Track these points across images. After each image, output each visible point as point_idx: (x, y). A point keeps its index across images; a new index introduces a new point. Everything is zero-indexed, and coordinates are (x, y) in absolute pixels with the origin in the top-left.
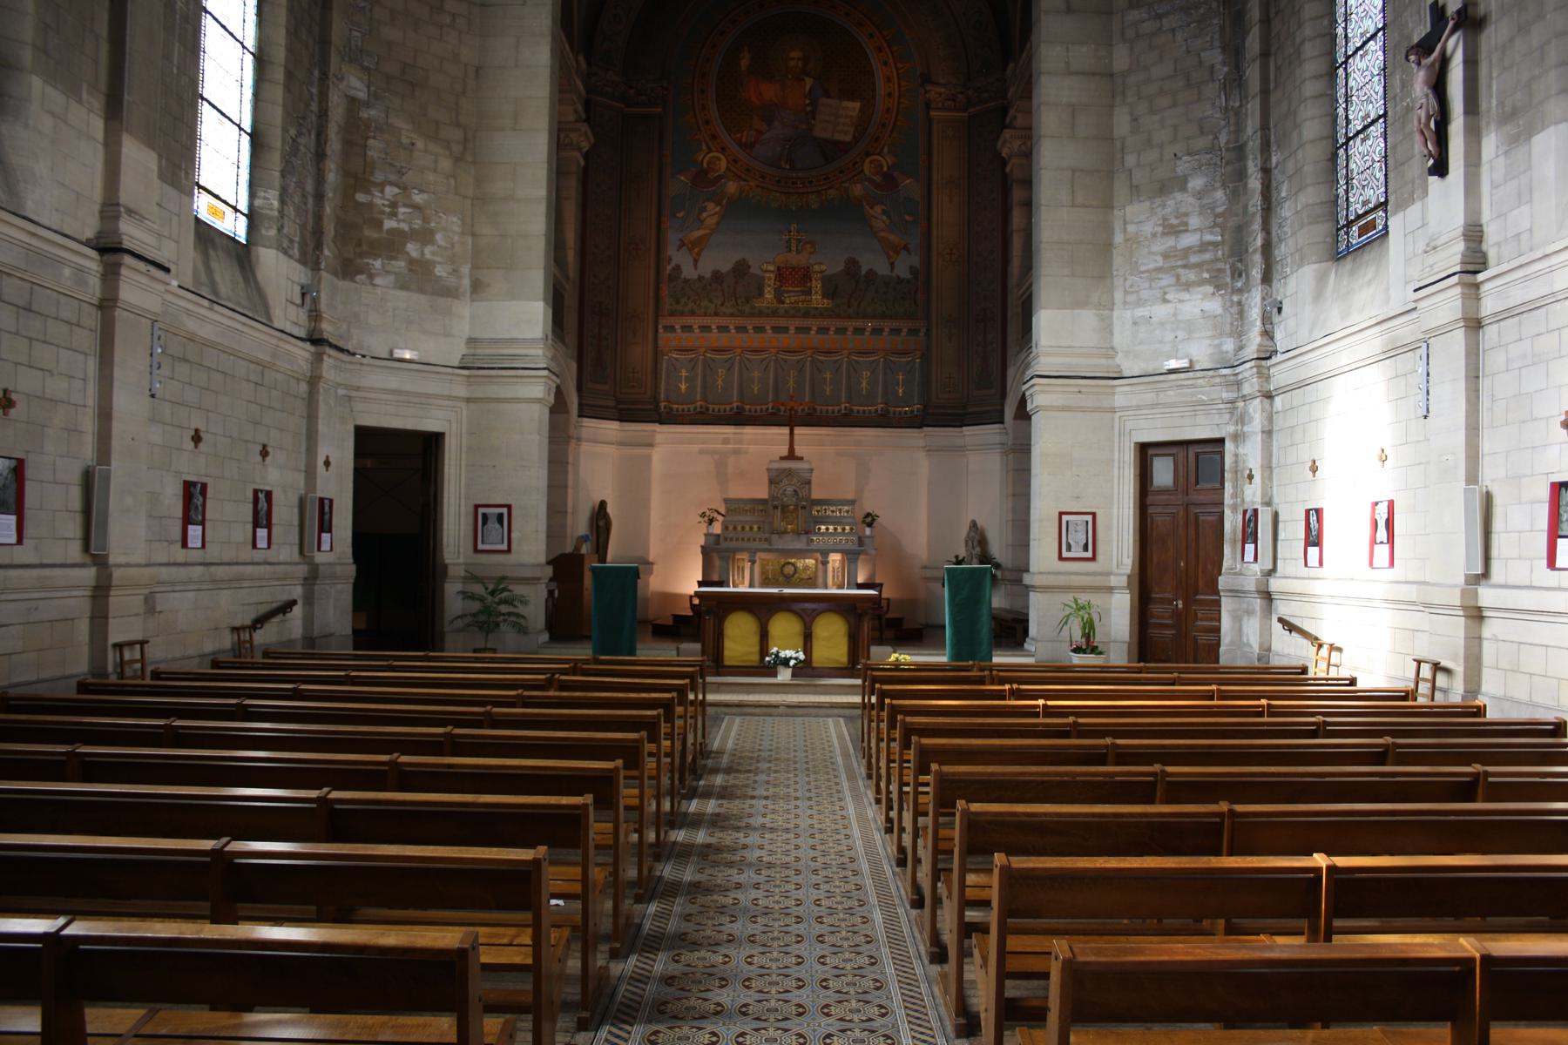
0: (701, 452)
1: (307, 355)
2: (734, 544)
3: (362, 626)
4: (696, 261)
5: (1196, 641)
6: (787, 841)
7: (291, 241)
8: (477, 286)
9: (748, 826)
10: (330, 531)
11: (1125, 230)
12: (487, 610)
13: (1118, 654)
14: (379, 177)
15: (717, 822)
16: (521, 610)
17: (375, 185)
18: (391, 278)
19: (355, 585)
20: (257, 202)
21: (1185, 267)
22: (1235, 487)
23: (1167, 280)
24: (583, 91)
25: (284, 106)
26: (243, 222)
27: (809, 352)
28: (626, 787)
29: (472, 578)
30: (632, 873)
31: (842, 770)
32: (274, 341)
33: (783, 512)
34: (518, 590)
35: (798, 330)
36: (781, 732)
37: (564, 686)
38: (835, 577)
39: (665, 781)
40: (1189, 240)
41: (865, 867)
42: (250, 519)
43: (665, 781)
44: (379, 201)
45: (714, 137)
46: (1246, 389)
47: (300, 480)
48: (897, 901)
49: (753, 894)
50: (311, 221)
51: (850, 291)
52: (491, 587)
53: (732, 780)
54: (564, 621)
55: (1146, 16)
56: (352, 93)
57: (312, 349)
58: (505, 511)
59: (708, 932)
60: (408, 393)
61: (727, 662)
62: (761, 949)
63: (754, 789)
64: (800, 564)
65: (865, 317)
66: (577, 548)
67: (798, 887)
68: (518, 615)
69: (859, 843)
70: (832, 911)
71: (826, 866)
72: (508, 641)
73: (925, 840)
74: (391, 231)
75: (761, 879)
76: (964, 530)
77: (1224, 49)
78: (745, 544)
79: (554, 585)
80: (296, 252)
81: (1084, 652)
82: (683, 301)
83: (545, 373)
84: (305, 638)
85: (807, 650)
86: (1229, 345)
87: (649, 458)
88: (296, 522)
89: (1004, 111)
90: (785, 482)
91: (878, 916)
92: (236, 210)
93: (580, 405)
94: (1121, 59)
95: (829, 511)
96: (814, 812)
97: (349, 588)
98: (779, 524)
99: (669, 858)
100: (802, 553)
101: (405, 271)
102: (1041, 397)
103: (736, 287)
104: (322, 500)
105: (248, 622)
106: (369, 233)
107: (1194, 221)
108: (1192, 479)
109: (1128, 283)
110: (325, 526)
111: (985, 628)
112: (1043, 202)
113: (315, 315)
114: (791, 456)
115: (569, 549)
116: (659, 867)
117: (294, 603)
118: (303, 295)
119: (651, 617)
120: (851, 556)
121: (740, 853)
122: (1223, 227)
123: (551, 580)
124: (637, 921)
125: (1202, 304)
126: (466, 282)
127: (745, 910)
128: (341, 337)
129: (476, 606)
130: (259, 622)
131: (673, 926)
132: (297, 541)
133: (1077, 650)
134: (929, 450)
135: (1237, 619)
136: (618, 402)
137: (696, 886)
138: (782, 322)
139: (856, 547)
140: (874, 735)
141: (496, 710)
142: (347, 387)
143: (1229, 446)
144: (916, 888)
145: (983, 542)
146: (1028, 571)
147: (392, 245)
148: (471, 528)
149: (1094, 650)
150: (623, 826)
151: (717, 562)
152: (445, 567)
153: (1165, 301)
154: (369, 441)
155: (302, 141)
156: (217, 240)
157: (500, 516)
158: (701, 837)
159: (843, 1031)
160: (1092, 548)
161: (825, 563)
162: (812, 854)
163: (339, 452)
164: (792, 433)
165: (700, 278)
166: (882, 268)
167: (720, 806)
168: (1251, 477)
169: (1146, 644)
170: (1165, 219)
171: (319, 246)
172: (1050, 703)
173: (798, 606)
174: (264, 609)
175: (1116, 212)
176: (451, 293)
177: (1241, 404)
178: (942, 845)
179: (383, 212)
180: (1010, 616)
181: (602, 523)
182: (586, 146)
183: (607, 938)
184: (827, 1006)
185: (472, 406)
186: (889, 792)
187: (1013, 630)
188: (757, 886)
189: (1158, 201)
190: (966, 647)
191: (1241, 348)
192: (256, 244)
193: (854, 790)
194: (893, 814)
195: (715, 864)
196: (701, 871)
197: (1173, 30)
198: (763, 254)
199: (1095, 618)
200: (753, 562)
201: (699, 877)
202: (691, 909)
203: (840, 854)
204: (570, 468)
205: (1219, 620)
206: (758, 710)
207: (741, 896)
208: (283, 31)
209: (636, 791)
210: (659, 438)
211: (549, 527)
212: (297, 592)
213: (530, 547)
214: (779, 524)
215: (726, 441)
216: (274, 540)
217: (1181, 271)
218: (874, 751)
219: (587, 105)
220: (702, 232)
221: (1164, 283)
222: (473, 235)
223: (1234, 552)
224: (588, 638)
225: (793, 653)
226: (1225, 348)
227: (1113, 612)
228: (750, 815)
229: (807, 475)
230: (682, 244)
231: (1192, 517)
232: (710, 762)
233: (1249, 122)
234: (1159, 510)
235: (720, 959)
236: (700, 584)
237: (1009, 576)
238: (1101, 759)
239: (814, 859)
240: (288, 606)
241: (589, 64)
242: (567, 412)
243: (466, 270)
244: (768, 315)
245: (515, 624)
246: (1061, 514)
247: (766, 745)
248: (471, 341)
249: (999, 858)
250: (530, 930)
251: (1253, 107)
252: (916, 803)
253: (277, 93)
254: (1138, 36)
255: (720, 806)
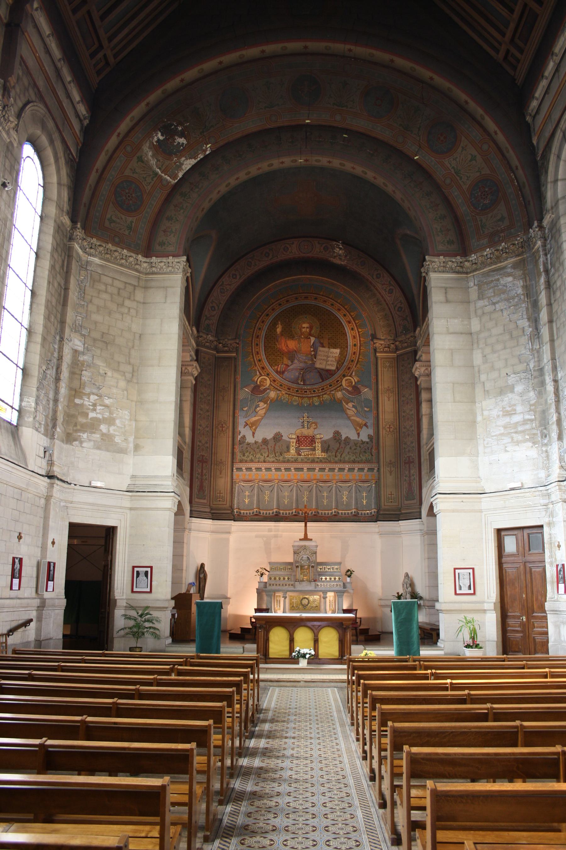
0: (257, 536)
1: (45, 484)
2: (274, 588)
3: (68, 632)
4: (254, 433)
5: (534, 639)
6: (306, 765)
7: (40, 424)
8: (137, 448)
9: (283, 756)
10: (53, 580)
11: (482, 414)
12: (138, 626)
13: (490, 646)
14: (87, 390)
15: (266, 753)
16: (156, 625)
17: (85, 394)
18: (92, 443)
19: (66, 611)
20: (24, 404)
21: (516, 432)
22: (551, 552)
23: (507, 440)
24: (195, 345)
25: (41, 355)
26: (16, 414)
27: (315, 482)
28: (215, 733)
29: (131, 607)
30: (217, 786)
31: (337, 720)
32: (28, 477)
33: (301, 569)
34: (155, 614)
35: (309, 469)
36: (301, 697)
37: (180, 673)
38: (331, 607)
39: (237, 728)
40: (517, 418)
41: (351, 782)
42: (10, 574)
43: (237, 728)
44: (86, 403)
45: (263, 368)
46: (554, 498)
47: (38, 552)
48: (371, 804)
49: (288, 799)
50: (51, 413)
51: (337, 448)
52: (140, 612)
53: (274, 726)
54: (180, 633)
55: (487, 304)
56: (76, 348)
57: (48, 481)
58: (149, 569)
59: (261, 825)
60: (98, 505)
61: (271, 656)
62: (293, 836)
63: (287, 732)
64: (311, 598)
65: (344, 462)
66: (188, 590)
67: (313, 794)
68: (154, 628)
69: (348, 766)
70: (333, 810)
71: (329, 781)
72: (149, 643)
73: (386, 767)
74: (92, 419)
75: (292, 789)
76: (402, 578)
77: (529, 319)
78: (280, 588)
79: (175, 611)
80: (42, 430)
81: (472, 647)
82: (247, 454)
83: (173, 494)
84: (36, 640)
85: (316, 648)
86: (542, 474)
87: (228, 540)
88: (35, 575)
89: (415, 352)
90: (302, 552)
91: (359, 814)
92: (12, 408)
93: (191, 511)
94: (475, 325)
95: (327, 568)
96: (321, 747)
97: (62, 612)
98: (299, 576)
99: (238, 777)
100: (312, 592)
101: (99, 440)
102: (441, 505)
103: (275, 447)
104: (49, 563)
105: (5, 632)
106: (82, 420)
107: (519, 408)
108: (527, 548)
109: (486, 442)
110: (50, 577)
111: (415, 634)
112: (438, 400)
113: (51, 463)
114: (306, 538)
115: (184, 591)
116: (232, 782)
117: (31, 620)
118: (45, 452)
119: (228, 628)
120: (339, 594)
121: (279, 773)
122: (535, 412)
123: (173, 608)
124: (219, 817)
125: (527, 452)
126: (131, 446)
127: (283, 810)
128: (64, 474)
129: (132, 623)
130: (12, 631)
131: (241, 820)
132: (35, 586)
133: (468, 646)
134: (381, 534)
135: (557, 627)
136: (212, 509)
137: (254, 794)
138: (300, 466)
139: (342, 589)
140: (354, 700)
141: (142, 688)
142: (66, 501)
143: (546, 529)
144: (382, 795)
145: (412, 585)
146: (438, 601)
147: (93, 426)
148: (130, 579)
149: (477, 646)
150: (212, 758)
151: (265, 598)
152: (115, 601)
153: (506, 451)
154: (76, 530)
155: (48, 372)
156: (2, 424)
157: (146, 573)
158: (257, 762)
159: (335, 839)
160: (473, 586)
161: (325, 598)
162: (321, 773)
163: (60, 537)
164: (306, 526)
165: (256, 442)
166: (353, 436)
167: (268, 743)
168: (559, 546)
169: (506, 645)
170: (503, 408)
171: (54, 426)
172: (454, 681)
173: (310, 624)
174: (14, 624)
175: (477, 405)
176: (123, 451)
177: (551, 506)
178: (396, 770)
179: (89, 409)
180: (428, 627)
181: (202, 576)
182: (196, 373)
183: (202, 828)
184: (328, 841)
185: (133, 512)
186: (364, 735)
187: (431, 635)
188: (289, 794)
189: (499, 398)
190: (405, 647)
191: (549, 476)
192: (22, 426)
193: (344, 732)
194: (367, 748)
195: (265, 780)
196: (257, 784)
197: (502, 310)
198: (288, 428)
199: (477, 628)
200: (285, 598)
201: (256, 788)
202: (251, 809)
203: (337, 773)
204: (185, 545)
205: (547, 628)
206: (288, 684)
207: (280, 801)
208: (42, 317)
209: (220, 736)
210: (233, 529)
211: (173, 578)
212: (33, 615)
213: (163, 591)
214: (299, 576)
215: (270, 530)
216: (22, 585)
217: (514, 435)
218: (355, 709)
219: (197, 352)
220: (257, 418)
221: (505, 441)
222: (136, 420)
223: (552, 588)
224: (194, 641)
225: (308, 651)
226: (540, 476)
227: (487, 623)
228: (285, 749)
229: (314, 549)
230: (247, 424)
231: (528, 569)
232: (261, 715)
233: (545, 356)
234: (509, 565)
235: (268, 842)
236: (257, 610)
237: (427, 603)
238: (484, 717)
239: (322, 777)
240: (28, 622)
241: (198, 331)
242: (184, 515)
243: (131, 439)
244: (292, 462)
245: (153, 634)
246: (455, 569)
247: (293, 705)
248: (133, 477)
249: (430, 783)
250: (158, 828)
251: (546, 348)
252: (380, 743)
253: (37, 348)
254: (484, 313)
255: (268, 743)
